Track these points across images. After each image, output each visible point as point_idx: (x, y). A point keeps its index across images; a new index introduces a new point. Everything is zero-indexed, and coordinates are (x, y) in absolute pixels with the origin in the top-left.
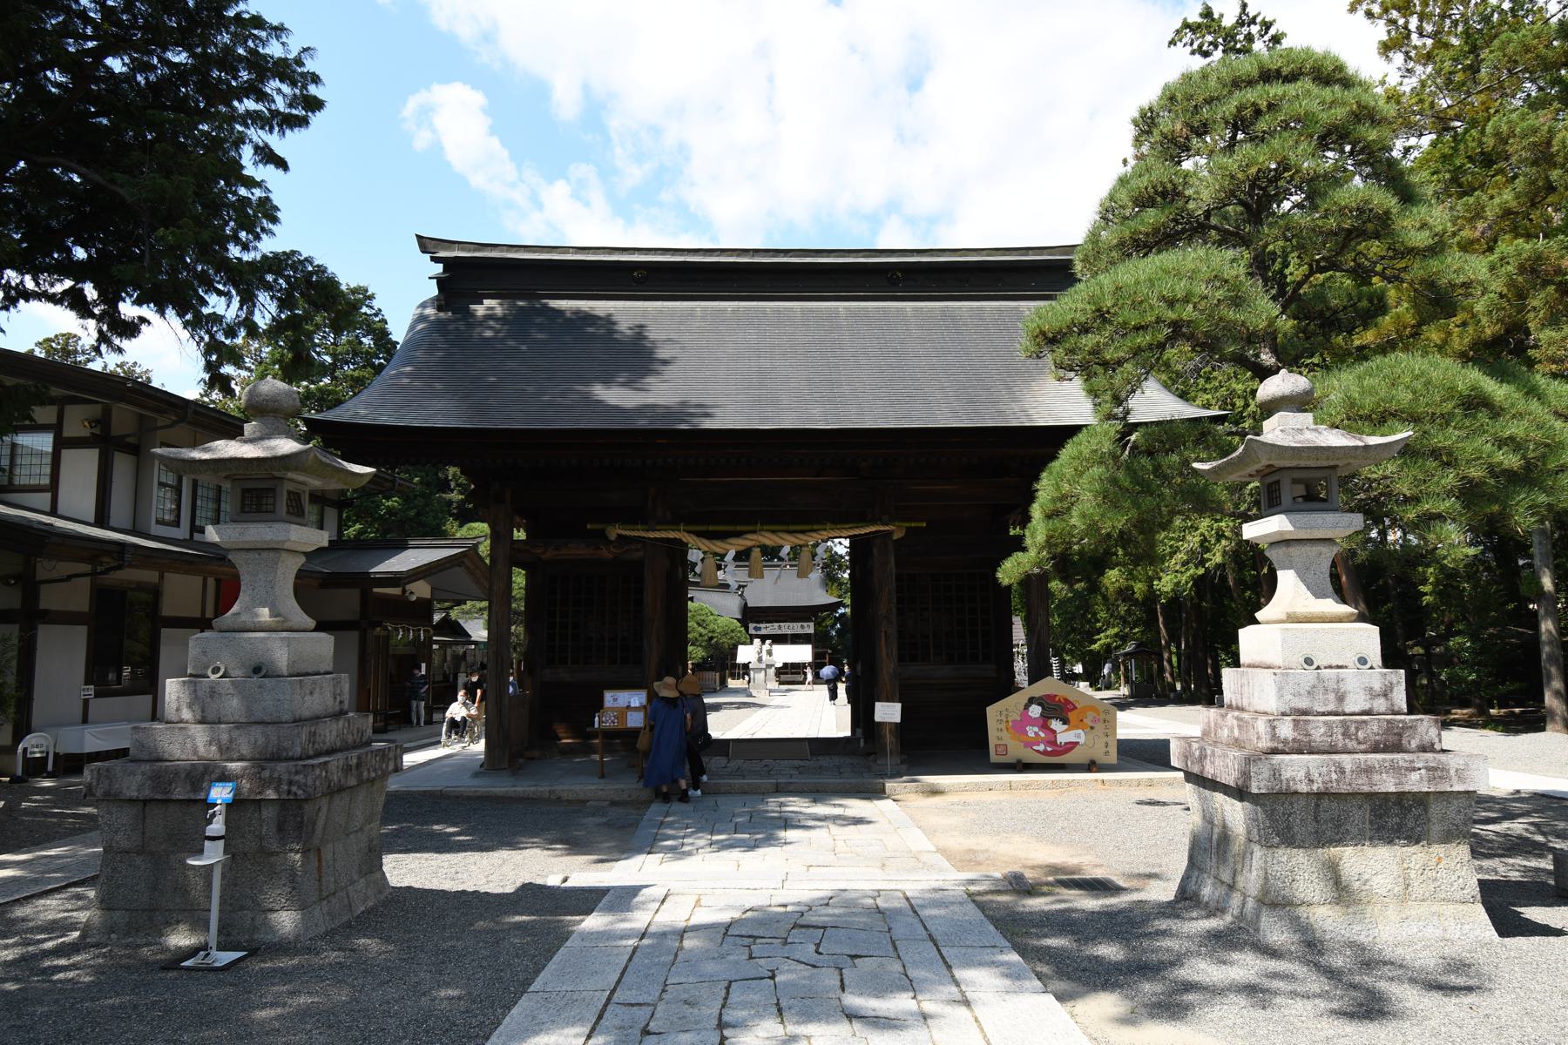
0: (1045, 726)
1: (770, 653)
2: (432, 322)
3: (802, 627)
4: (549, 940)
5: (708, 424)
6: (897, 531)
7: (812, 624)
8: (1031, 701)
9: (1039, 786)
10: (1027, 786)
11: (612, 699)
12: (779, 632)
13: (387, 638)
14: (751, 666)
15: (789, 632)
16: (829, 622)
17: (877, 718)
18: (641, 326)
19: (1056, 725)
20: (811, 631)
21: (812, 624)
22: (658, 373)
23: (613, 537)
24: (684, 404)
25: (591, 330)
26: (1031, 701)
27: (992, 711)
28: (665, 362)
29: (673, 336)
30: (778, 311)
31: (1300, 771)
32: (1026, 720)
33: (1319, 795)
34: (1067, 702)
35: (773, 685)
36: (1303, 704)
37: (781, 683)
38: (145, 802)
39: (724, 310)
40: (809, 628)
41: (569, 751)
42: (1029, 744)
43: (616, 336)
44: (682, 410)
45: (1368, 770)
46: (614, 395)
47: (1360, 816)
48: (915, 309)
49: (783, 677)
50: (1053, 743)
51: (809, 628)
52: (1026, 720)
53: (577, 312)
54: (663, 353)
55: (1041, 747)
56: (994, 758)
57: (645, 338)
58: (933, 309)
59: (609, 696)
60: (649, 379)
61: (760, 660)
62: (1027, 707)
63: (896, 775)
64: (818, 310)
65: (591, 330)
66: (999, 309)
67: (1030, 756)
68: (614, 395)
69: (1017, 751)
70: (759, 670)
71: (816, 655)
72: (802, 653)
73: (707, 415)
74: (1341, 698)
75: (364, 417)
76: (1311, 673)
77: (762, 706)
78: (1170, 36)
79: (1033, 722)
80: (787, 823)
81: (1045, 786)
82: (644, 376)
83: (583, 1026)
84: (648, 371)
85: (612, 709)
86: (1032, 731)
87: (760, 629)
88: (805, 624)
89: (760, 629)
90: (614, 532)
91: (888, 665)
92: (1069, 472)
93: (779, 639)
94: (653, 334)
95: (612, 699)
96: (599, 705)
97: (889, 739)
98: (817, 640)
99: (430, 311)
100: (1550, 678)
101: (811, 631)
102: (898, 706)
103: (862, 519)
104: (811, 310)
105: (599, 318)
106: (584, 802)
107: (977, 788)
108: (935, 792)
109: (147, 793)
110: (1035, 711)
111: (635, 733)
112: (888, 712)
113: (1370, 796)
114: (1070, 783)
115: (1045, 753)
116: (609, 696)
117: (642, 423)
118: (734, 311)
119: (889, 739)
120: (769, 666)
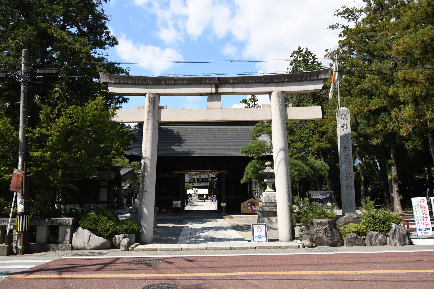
0: (251, 207)
1: (197, 191)
2: (138, 131)
3: (206, 184)
4: (181, 230)
5: (194, 155)
6: (225, 172)
7: (208, 183)
8: (249, 202)
9: (249, 217)
10: (247, 217)
11: (174, 202)
12: (199, 185)
13: (114, 189)
14: (192, 195)
15: (202, 185)
16: (213, 182)
17: (221, 205)
18: (179, 132)
19: (253, 207)
20: (208, 185)
21: (208, 183)
22: (183, 143)
23: (175, 173)
24: (189, 150)
25: (169, 133)
26: (249, 202)
27: (242, 204)
28: (184, 141)
29: (184, 134)
30: (204, 128)
31: (266, 208)
32: (248, 206)
33: (267, 211)
34: (255, 203)
35: (198, 200)
36: (267, 201)
37: (200, 200)
38: (135, 213)
39: (193, 128)
40: (208, 184)
41: (165, 212)
42: (248, 210)
43: (174, 134)
44: (189, 152)
45: (272, 209)
46: (176, 148)
47: (271, 214)
48: (230, 128)
49: (200, 198)
50: (252, 210)
51: (208, 184)
52: (248, 206)
53: (166, 128)
54: (183, 139)
55: (250, 211)
56: (242, 212)
57: (179, 135)
58: (233, 128)
59: (174, 202)
60: (182, 145)
61: (195, 193)
62: (248, 204)
63: (225, 215)
64: (211, 128)
65: (169, 133)
66: (246, 128)
67: (248, 212)
68: (176, 148)
69: (246, 211)
70: (195, 196)
71: (209, 192)
72: (205, 191)
73: (194, 153)
74: (271, 201)
75: (133, 154)
76: (268, 198)
77: (196, 205)
78: (291, 55)
79: (249, 206)
80: (207, 221)
81: (250, 217)
82: (181, 144)
83: (260, 141)
84: (182, 143)
85: (175, 204)
86: (249, 208)
87: (193, 184)
88: (206, 183)
89: (193, 184)
90: (175, 172)
91: (224, 196)
92: (249, 168)
93: (199, 187)
94: (181, 134)
95: (174, 202)
96: (172, 203)
97: (224, 209)
98: (210, 188)
99: (137, 128)
100: (362, 198)
101: (208, 185)
102: (225, 203)
103: (219, 170)
104: (210, 128)
105: (170, 130)
106: (171, 220)
107: (238, 217)
108: (232, 218)
109: (136, 212)
110: (249, 204)
111: (179, 208)
112: (223, 204)
113: (273, 211)
114: (254, 216)
115: (251, 212)
116: (174, 202)
117: (182, 155)
118: (196, 128)
119: (224, 209)
120: (197, 195)
